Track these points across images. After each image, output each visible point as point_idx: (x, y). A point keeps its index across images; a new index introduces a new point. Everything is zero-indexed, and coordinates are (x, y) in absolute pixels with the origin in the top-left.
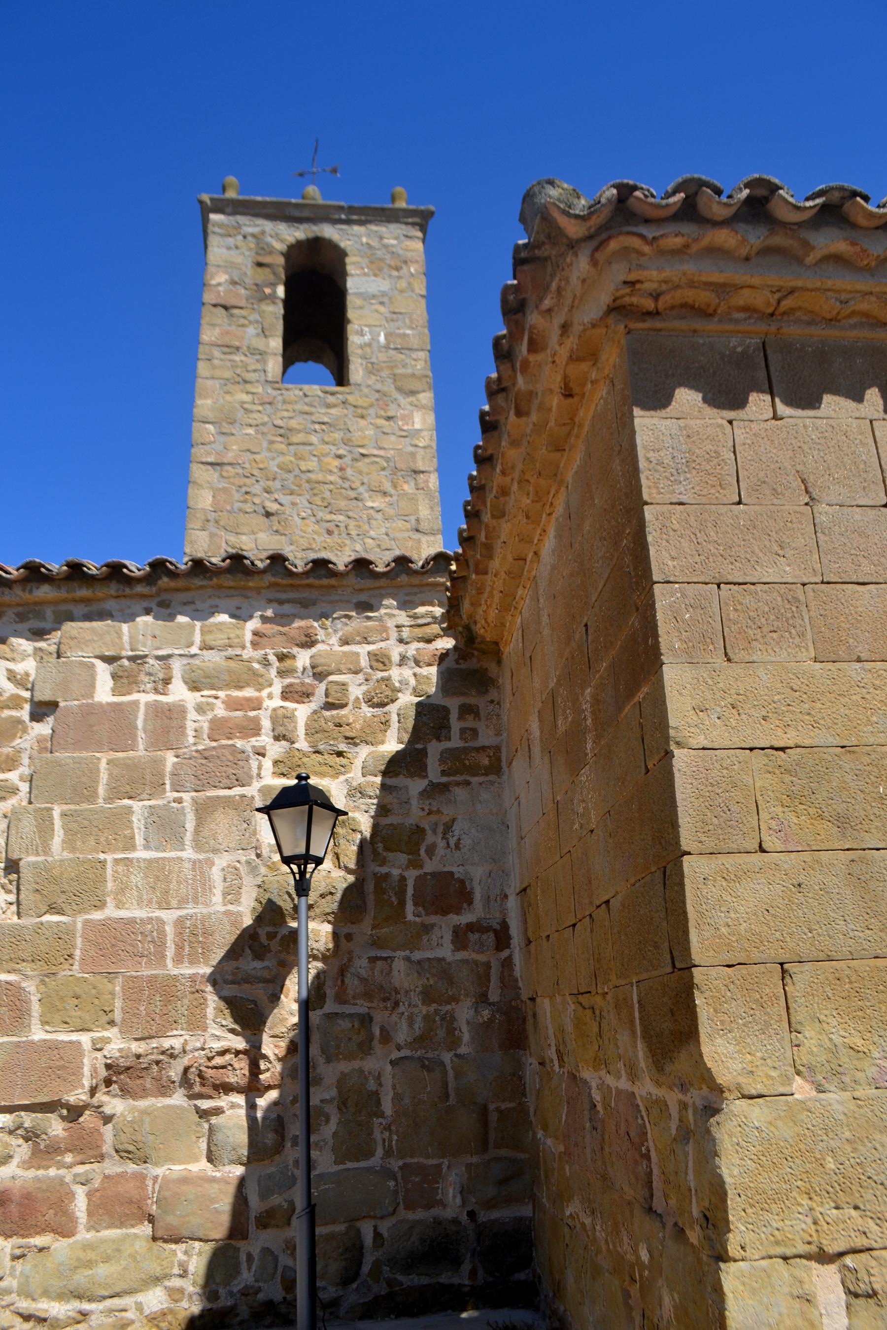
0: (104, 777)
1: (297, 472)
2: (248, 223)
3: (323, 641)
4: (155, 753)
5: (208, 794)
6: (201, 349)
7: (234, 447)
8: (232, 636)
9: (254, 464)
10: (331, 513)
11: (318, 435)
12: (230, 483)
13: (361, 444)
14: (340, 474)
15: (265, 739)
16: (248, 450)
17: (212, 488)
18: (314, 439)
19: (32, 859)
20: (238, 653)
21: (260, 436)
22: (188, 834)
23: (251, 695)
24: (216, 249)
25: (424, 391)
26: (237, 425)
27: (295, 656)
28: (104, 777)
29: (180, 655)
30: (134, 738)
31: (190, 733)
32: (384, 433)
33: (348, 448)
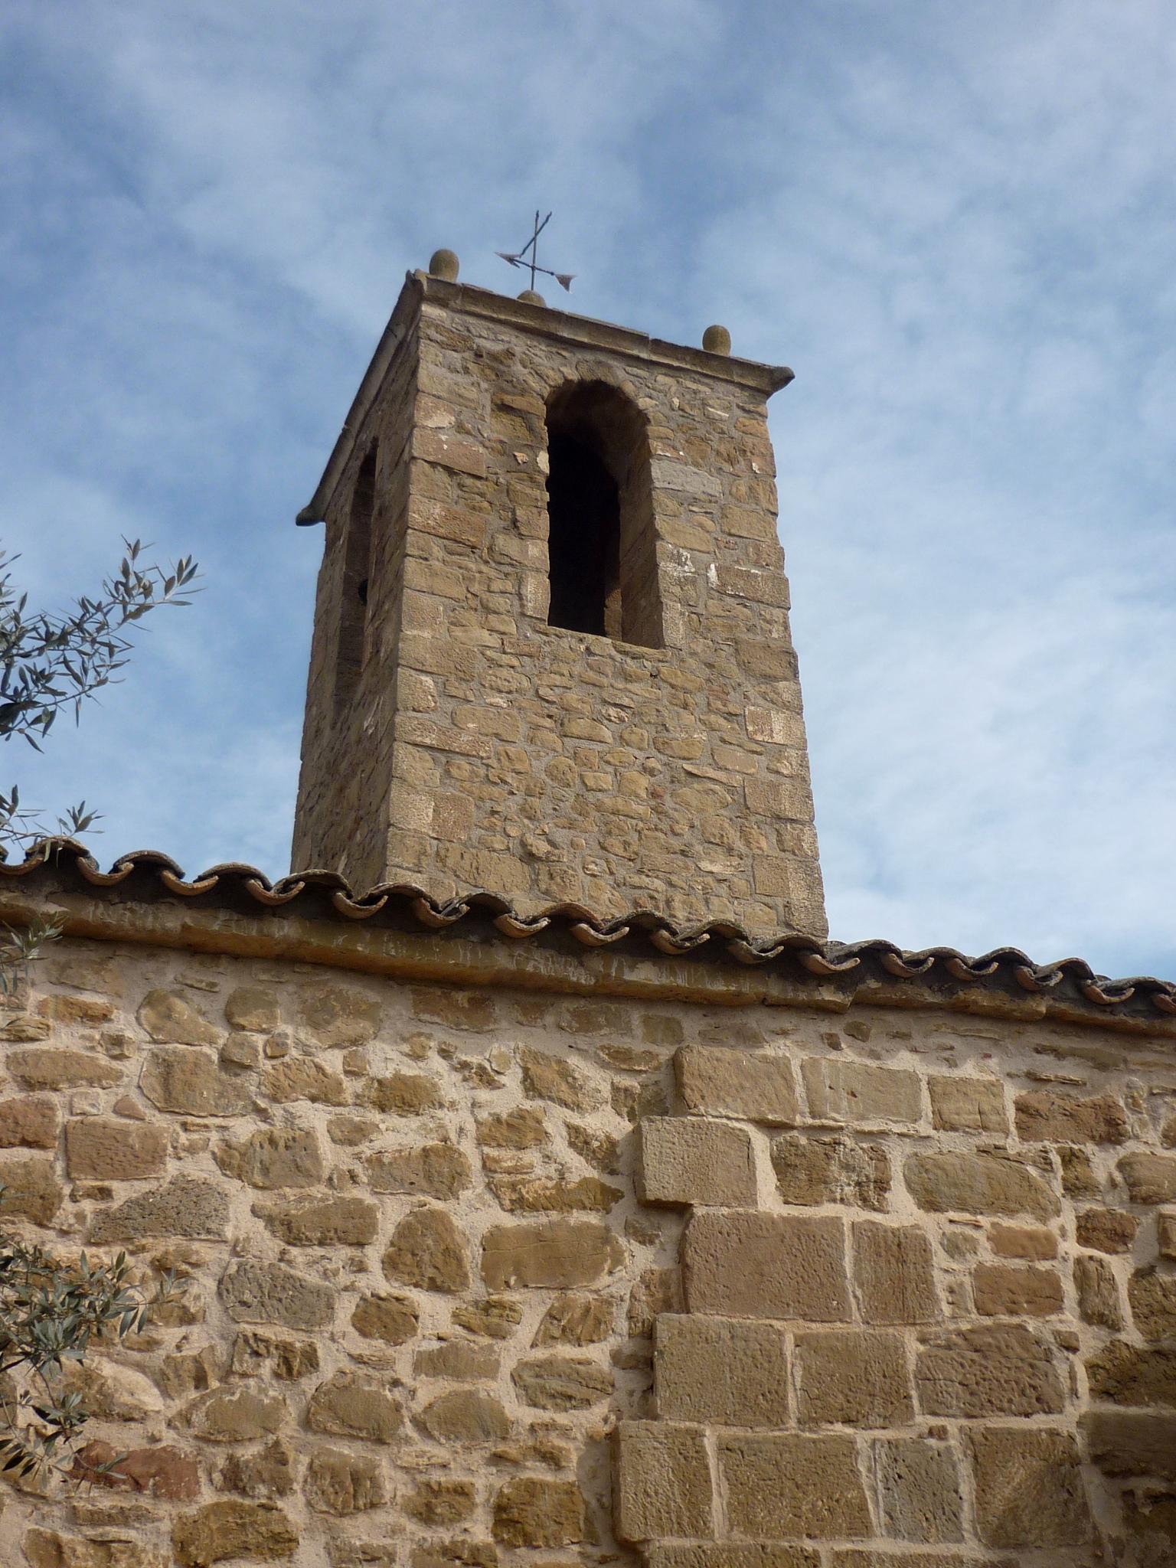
0: (796, 1375)
1: (578, 787)
2: (484, 333)
3: (1137, 1137)
4: (883, 1331)
5: (990, 1425)
6: (411, 537)
7: (471, 725)
8: (986, 1108)
9: (505, 762)
10: (640, 872)
11: (612, 726)
12: (463, 790)
13: (686, 755)
14: (653, 803)
15: (1069, 1320)
16: (497, 735)
17: (432, 794)
18: (607, 734)
19: (671, 1542)
20: (1001, 1143)
21: (515, 712)
22: (966, 1507)
23: (1034, 1228)
24: (432, 367)
25: (786, 679)
26: (474, 685)
27: (1088, 1160)
28: (796, 1375)
29: (901, 1135)
30: (840, 1293)
31: (943, 1295)
32: (724, 741)
33: (664, 758)
